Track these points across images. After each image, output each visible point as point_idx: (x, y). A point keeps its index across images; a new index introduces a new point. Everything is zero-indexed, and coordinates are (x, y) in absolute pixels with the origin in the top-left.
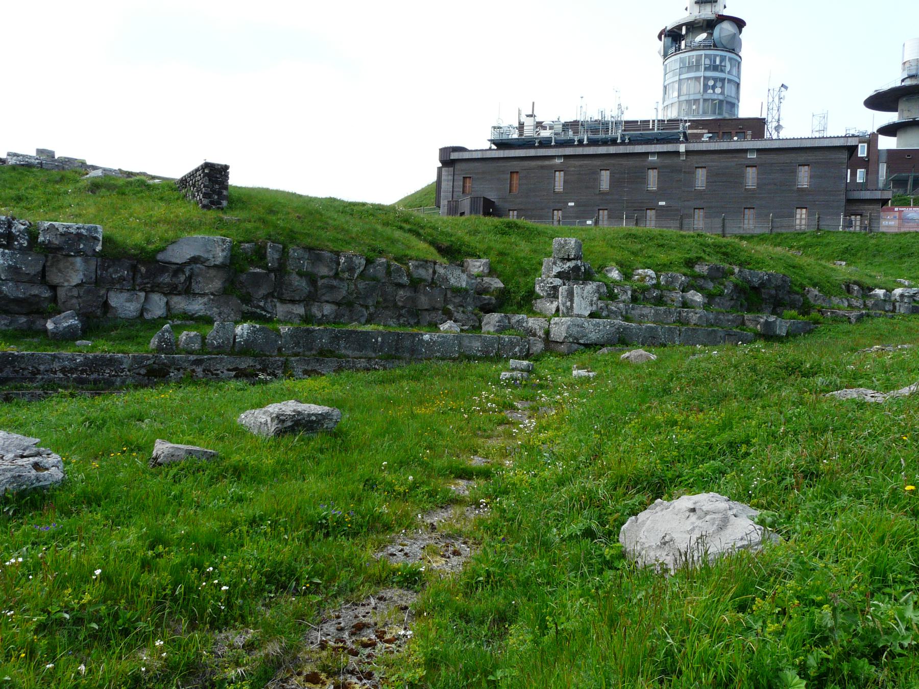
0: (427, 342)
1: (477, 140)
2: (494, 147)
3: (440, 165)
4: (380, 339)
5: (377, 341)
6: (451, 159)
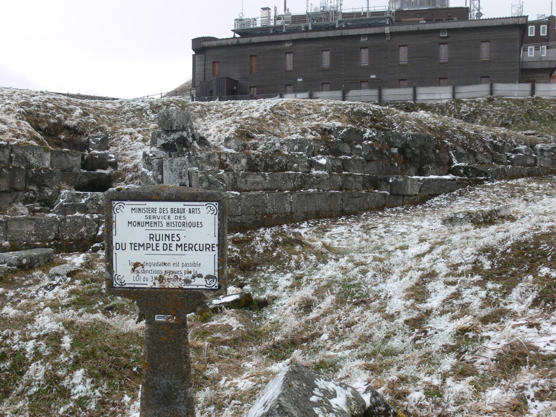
1: (224, 31)
2: (237, 36)
3: (194, 53)
6: (203, 48)
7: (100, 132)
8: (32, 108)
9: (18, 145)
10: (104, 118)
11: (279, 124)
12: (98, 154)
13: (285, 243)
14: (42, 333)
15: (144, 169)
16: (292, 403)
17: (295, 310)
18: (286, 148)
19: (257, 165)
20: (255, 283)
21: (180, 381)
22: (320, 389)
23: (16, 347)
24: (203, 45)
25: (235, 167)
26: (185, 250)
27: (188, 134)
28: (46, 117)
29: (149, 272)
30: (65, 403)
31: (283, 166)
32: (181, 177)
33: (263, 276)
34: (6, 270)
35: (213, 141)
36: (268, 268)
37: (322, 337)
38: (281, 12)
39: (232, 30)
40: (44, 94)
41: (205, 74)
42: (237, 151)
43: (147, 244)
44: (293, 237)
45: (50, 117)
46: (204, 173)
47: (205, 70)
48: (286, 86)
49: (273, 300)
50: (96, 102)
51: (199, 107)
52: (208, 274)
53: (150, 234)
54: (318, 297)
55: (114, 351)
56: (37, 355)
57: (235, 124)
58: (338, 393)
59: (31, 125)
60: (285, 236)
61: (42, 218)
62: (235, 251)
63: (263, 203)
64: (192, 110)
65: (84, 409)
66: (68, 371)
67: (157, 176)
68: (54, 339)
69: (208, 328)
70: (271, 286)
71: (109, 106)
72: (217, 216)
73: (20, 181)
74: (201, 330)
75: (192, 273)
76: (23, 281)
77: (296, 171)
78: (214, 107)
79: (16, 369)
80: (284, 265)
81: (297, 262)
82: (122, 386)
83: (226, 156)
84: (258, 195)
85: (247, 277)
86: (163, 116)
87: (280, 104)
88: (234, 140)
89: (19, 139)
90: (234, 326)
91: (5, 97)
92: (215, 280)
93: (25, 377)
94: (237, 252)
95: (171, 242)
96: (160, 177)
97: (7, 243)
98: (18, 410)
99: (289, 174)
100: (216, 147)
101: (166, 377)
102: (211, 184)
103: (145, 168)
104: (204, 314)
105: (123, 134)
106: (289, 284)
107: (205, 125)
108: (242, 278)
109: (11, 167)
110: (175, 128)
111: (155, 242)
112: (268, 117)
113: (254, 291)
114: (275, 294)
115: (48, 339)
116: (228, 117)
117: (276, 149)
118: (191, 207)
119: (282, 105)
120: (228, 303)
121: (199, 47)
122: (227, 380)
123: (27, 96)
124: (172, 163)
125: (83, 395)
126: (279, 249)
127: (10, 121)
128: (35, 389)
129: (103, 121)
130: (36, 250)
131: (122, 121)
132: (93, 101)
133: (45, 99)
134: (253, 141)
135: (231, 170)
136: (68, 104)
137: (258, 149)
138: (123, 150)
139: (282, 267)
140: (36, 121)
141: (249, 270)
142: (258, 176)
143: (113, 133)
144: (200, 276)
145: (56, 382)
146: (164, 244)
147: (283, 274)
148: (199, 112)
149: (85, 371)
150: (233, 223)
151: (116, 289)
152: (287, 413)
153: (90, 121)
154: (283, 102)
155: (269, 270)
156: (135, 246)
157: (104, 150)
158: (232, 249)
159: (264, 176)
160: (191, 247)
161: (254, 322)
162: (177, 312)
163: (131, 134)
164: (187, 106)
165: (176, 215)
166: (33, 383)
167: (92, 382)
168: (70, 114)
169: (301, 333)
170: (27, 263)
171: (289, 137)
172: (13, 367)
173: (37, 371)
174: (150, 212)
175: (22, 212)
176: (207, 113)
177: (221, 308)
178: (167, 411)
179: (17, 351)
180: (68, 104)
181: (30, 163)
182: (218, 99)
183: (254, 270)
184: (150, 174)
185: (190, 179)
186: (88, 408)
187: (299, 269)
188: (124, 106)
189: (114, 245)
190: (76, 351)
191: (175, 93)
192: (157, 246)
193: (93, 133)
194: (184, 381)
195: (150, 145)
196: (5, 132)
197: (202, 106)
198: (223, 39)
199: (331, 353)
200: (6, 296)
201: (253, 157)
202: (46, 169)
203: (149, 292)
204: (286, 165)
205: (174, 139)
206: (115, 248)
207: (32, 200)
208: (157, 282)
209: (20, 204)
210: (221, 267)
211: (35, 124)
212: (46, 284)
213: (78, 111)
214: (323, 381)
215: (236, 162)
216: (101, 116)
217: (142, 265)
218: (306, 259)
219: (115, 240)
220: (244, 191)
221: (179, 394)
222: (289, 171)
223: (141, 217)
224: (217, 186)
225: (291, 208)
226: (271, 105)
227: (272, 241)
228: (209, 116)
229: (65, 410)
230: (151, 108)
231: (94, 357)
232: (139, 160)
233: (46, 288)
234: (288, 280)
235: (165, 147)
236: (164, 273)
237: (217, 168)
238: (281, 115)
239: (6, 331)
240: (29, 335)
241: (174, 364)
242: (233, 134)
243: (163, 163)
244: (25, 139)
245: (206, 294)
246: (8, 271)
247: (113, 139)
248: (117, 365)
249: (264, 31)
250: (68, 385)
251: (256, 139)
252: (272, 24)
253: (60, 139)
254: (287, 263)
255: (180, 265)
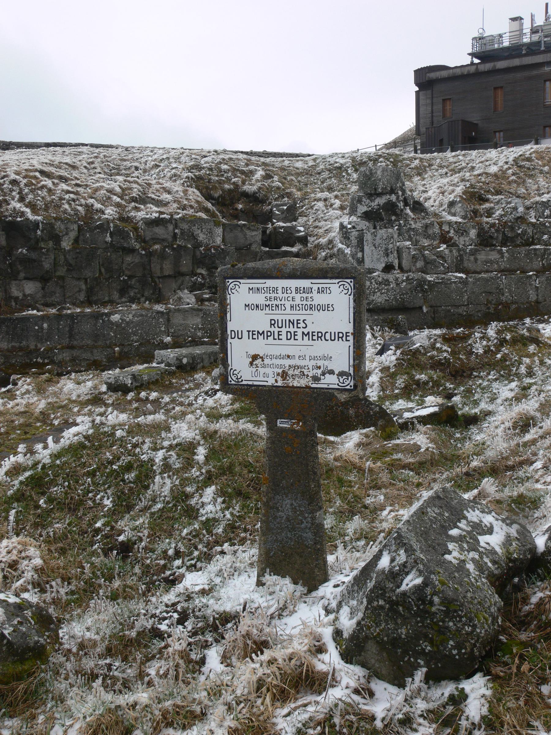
0: (117, 324)
1: (457, 55)
2: (476, 61)
3: (417, 89)
4: (45, 325)
5: (42, 328)
6: (430, 82)
7: (286, 199)
8: (203, 171)
9: (183, 219)
10: (292, 180)
11: (524, 181)
12: (283, 227)
13: (515, 341)
14: (175, 442)
15: (340, 246)
16: (417, 533)
17: (509, 429)
18: (533, 214)
19: (491, 237)
20: (469, 392)
21: (307, 503)
22: (469, 522)
23: (144, 457)
24: (429, 77)
25: (461, 241)
26: (313, 340)
27: (398, 198)
28: (219, 182)
29: (269, 366)
30: (190, 524)
31: (528, 239)
32: (387, 255)
33: (480, 384)
34: (163, 371)
35: (433, 206)
36: (489, 374)
37: (535, 465)
38: (540, 21)
39: (469, 54)
40: (218, 154)
41: (432, 116)
42: (464, 219)
43: (267, 332)
44: (527, 334)
45: (224, 182)
46: (419, 250)
47: (432, 112)
48: (545, 127)
49: (486, 415)
50: (284, 161)
51: (417, 161)
52: (341, 370)
53: (271, 320)
54: (543, 414)
55: (256, 467)
56: (166, 467)
57: (463, 183)
58: (496, 529)
59: (201, 193)
60: (516, 332)
61: (211, 308)
62: (445, 351)
63: (497, 288)
64: (408, 165)
65: (210, 532)
66: (198, 487)
67: (356, 254)
68: (187, 449)
69: (389, 447)
70: (488, 397)
71: (299, 165)
72: (352, 297)
73: (186, 263)
74: (381, 449)
75: (322, 369)
76: (182, 385)
77: (546, 245)
78: (438, 161)
79: (141, 482)
80: (510, 371)
81: (529, 368)
82: (258, 509)
83: (450, 226)
84: (492, 278)
85: (458, 385)
86: (365, 175)
87: (528, 153)
88: (460, 205)
89: (185, 212)
90: (422, 446)
91: (171, 160)
92: (350, 378)
93: (150, 492)
94: (447, 352)
95: (296, 329)
96: (360, 255)
97: (169, 339)
98: (137, 527)
99: (535, 250)
100: (436, 215)
101: (290, 496)
102: (428, 263)
103: (343, 244)
104: (387, 429)
105: (315, 200)
106: (510, 395)
107: (424, 185)
108: (452, 386)
109: (175, 246)
110: (380, 190)
111: (277, 330)
112: (510, 171)
113: (465, 403)
114: (491, 408)
115: (180, 449)
116: (456, 173)
117: (518, 215)
118: (320, 286)
119: (530, 154)
120: (423, 417)
121: (424, 81)
122: (391, 511)
123: (197, 157)
124: (376, 236)
125: (211, 516)
126: (505, 350)
127: (176, 189)
128: (159, 506)
129: (291, 185)
130: (200, 347)
131: (315, 183)
132: (280, 159)
133: (218, 160)
134: (487, 205)
135: (455, 245)
136: (247, 165)
137: (494, 216)
138: (315, 221)
139: (506, 371)
140: (207, 188)
141: (462, 376)
142: (492, 253)
143: (303, 199)
144: (331, 372)
145: (183, 500)
146: (287, 332)
147: (507, 382)
148: (416, 168)
149: (217, 489)
150: (456, 316)
151: (231, 387)
152: (405, 544)
153: (274, 185)
154: (532, 150)
155: (490, 377)
156: (254, 334)
157: (291, 222)
158: (441, 348)
159: (501, 252)
160: (321, 336)
161: (455, 443)
162: (304, 416)
163: (325, 200)
164: (401, 161)
165: (302, 295)
166: (158, 500)
167: (224, 502)
168: (249, 177)
169: (507, 458)
170: (188, 362)
171: (537, 199)
172: (138, 479)
173: (163, 486)
174: (271, 292)
175: (188, 300)
176: (428, 169)
177: (412, 423)
178: (291, 539)
179: (145, 461)
180: (247, 165)
181: (197, 240)
182: (449, 150)
183: (470, 376)
184: (348, 251)
185: (399, 257)
186: (214, 532)
187: (531, 376)
188: (318, 164)
189: (229, 332)
190: (210, 465)
191: (395, 144)
192: (279, 335)
193: (278, 201)
194: (311, 503)
195: (349, 213)
196: (169, 203)
197: (421, 160)
198: (456, 67)
199: (538, 486)
200: (161, 402)
201: (486, 227)
202: (217, 248)
203: (269, 390)
204: (533, 237)
205: (379, 205)
206: (229, 337)
207: (201, 287)
208: (279, 379)
209: (186, 291)
210: (357, 362)
211: (207, 191)
212: (208, 388)
213: (260, 173)
214: (477, 512)
215: (462, 234)
216: (289, 178)
217: (262, 358)
218: (542, 363)
219: (231, 326)
220: (473, 273)
221: (305, 518)
222: (536, 245)
223: (259, 299)
224: (435, 266)
225: (537, 295)
226: (515, 155)
227: (497, 338)
228: (430, 173)
229: (189, 531)
230: (353, 166)
231: (231, 473)
232: (335, 234)
233: (206, 393)
234: (511, 390)
235: (367, 216)
236: (287, 368)
237: (437, 242)
238: (529, 169)
239: (136, 438)
240: (160, 444)
241: (299, 481)
242: (460, 196)
243: (363, 236)
244: (193, 210)
245: (338, 396)
246: (165, 372)
247: (302, 207)
248: (257, 484)
249: (515, 51)
250: (197, 504)
251: (492, 202)
252: (526, 40)
253: (236, 209)
254: (515, 369)
255: (307, 358)
